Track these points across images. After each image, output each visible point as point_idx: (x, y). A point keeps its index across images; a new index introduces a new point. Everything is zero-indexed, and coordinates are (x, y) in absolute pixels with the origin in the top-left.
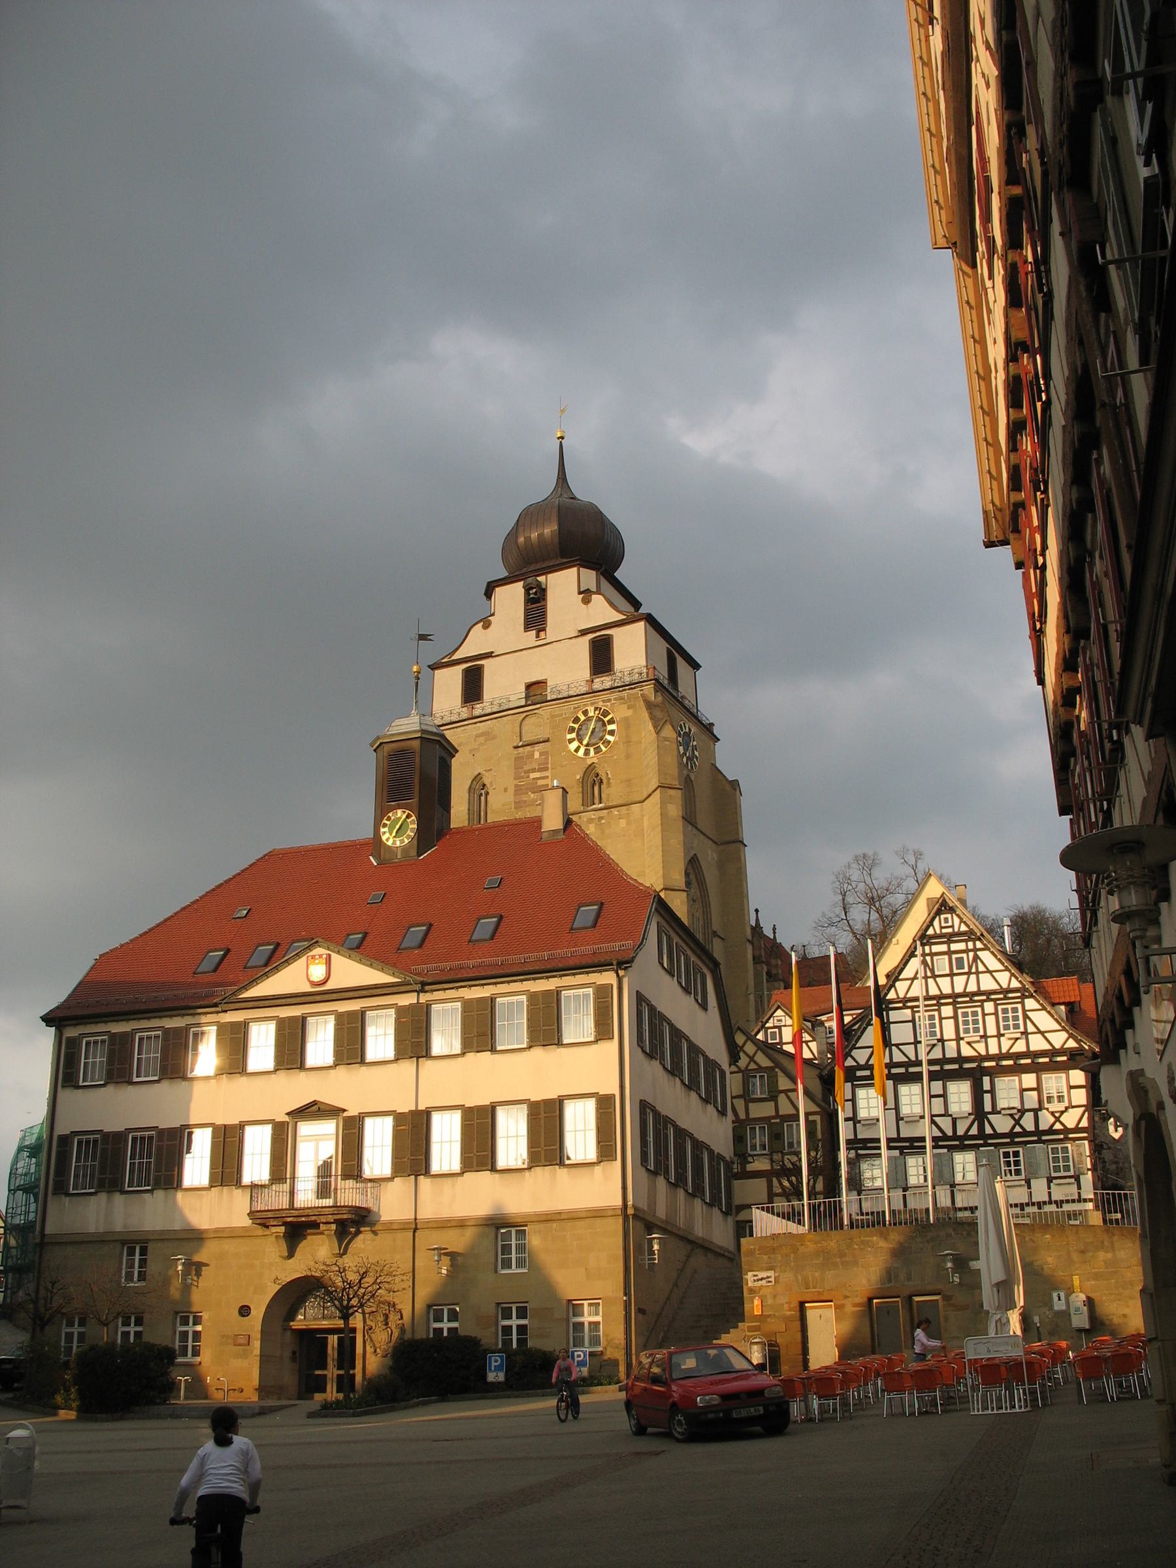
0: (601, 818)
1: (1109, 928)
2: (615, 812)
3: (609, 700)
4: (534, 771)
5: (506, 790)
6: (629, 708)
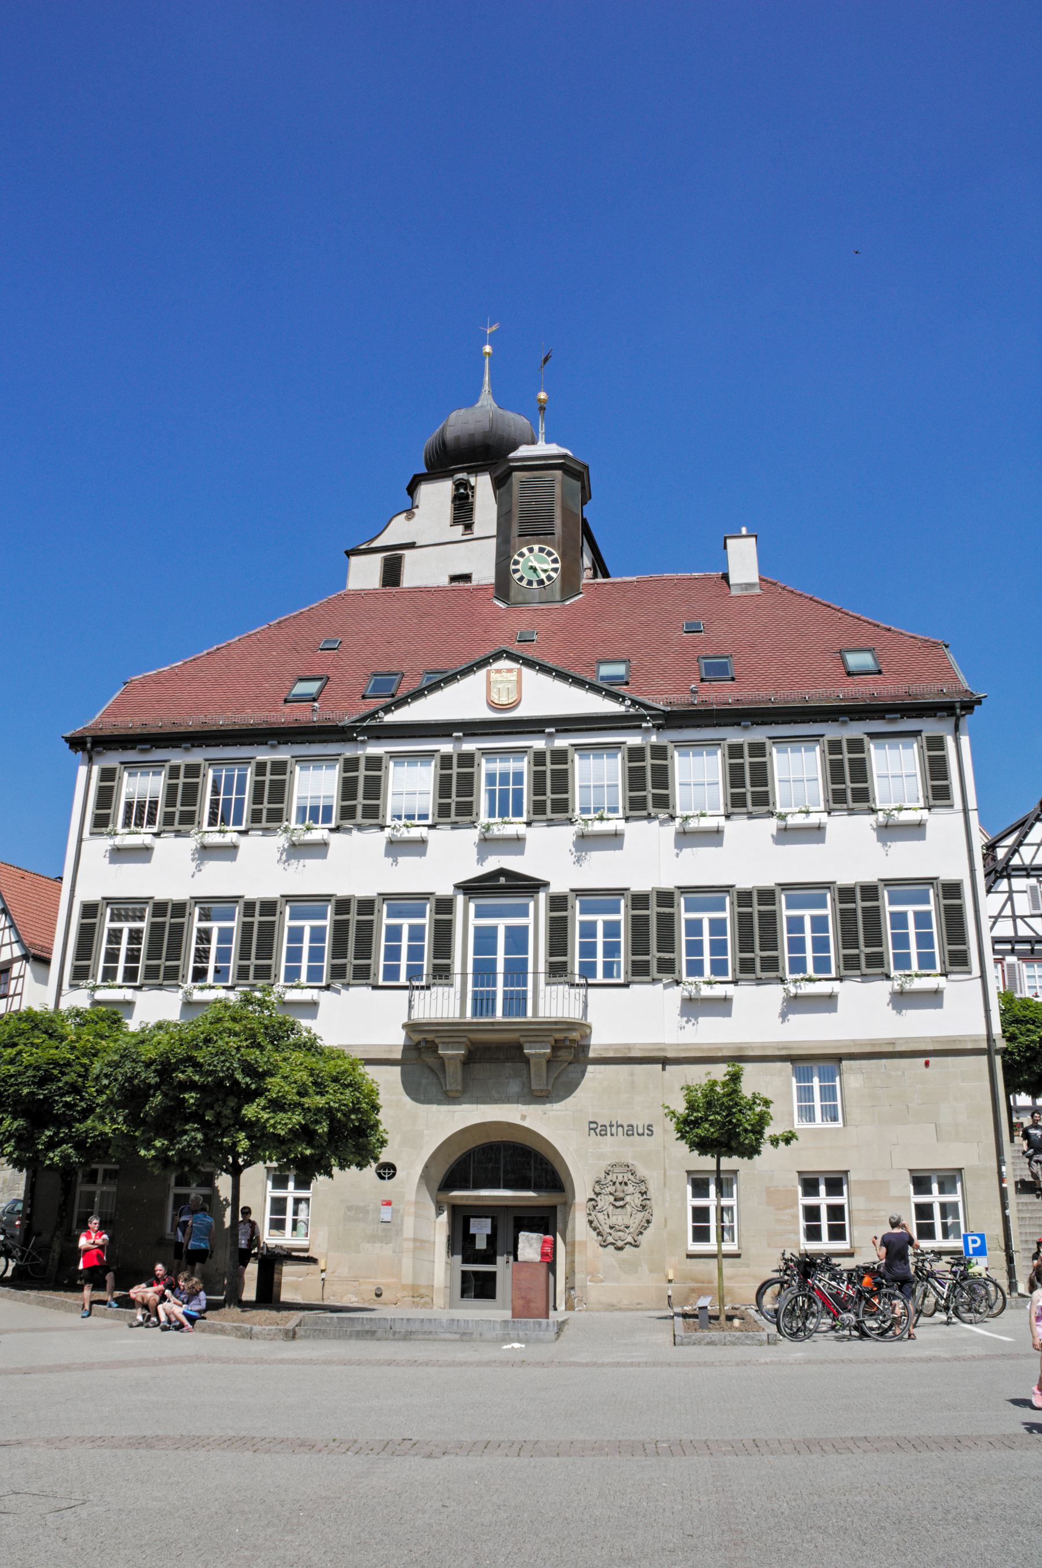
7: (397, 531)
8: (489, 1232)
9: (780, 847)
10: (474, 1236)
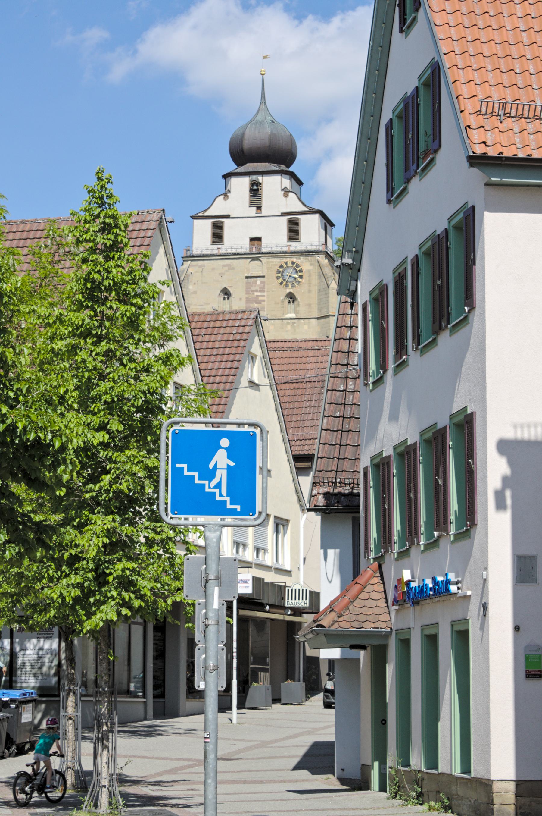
0: (294, 323)
1: (293, 757)
4: (257, 291)
5: (241, 299)
6: (311, 265)
7: (219, 207)
8: (266, 581)
9: (231, 292)
10: (321, 548)
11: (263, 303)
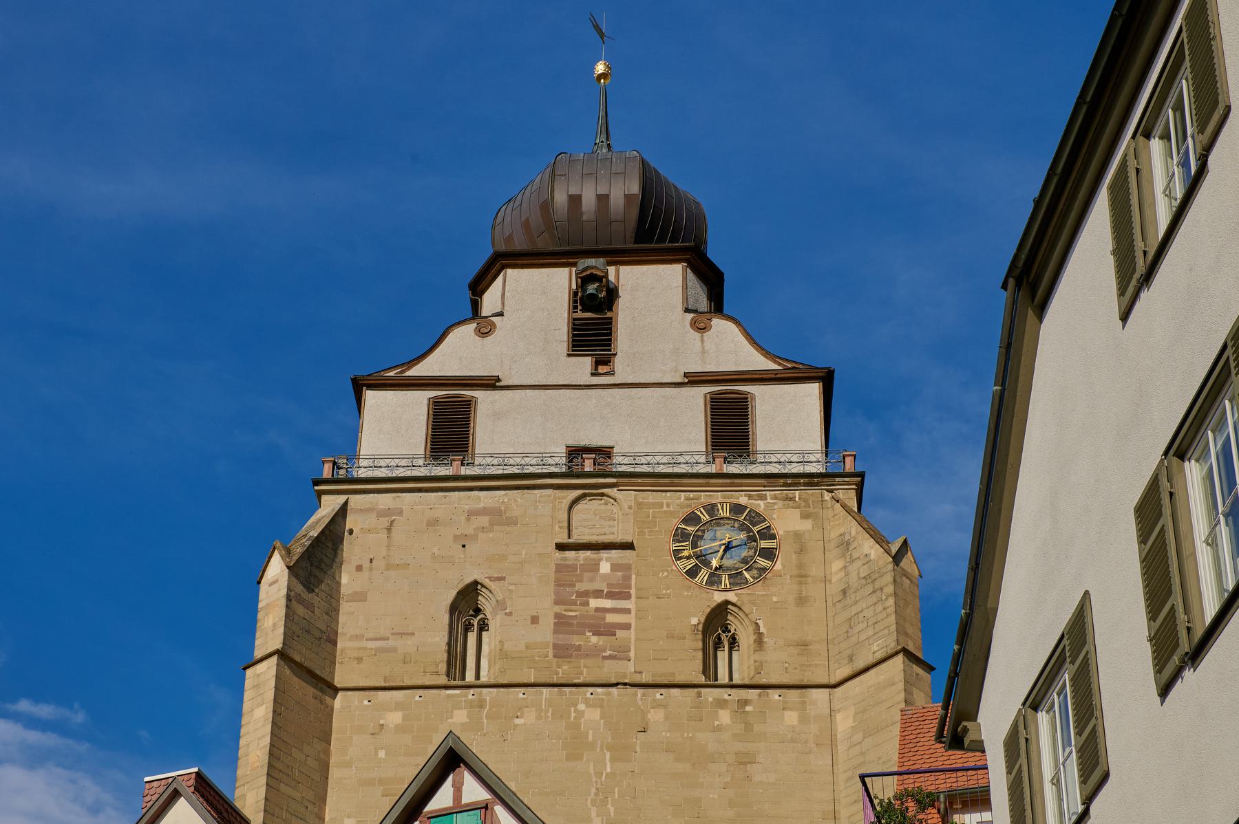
2: (774, 695)
3: (763, 498)
4: (598, 594)
5: (535, 620)
6: (805, 516)
11: (620, 633)
